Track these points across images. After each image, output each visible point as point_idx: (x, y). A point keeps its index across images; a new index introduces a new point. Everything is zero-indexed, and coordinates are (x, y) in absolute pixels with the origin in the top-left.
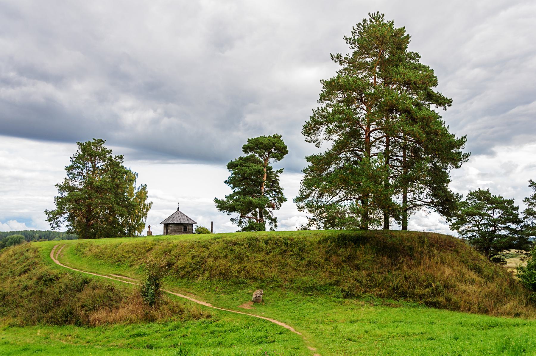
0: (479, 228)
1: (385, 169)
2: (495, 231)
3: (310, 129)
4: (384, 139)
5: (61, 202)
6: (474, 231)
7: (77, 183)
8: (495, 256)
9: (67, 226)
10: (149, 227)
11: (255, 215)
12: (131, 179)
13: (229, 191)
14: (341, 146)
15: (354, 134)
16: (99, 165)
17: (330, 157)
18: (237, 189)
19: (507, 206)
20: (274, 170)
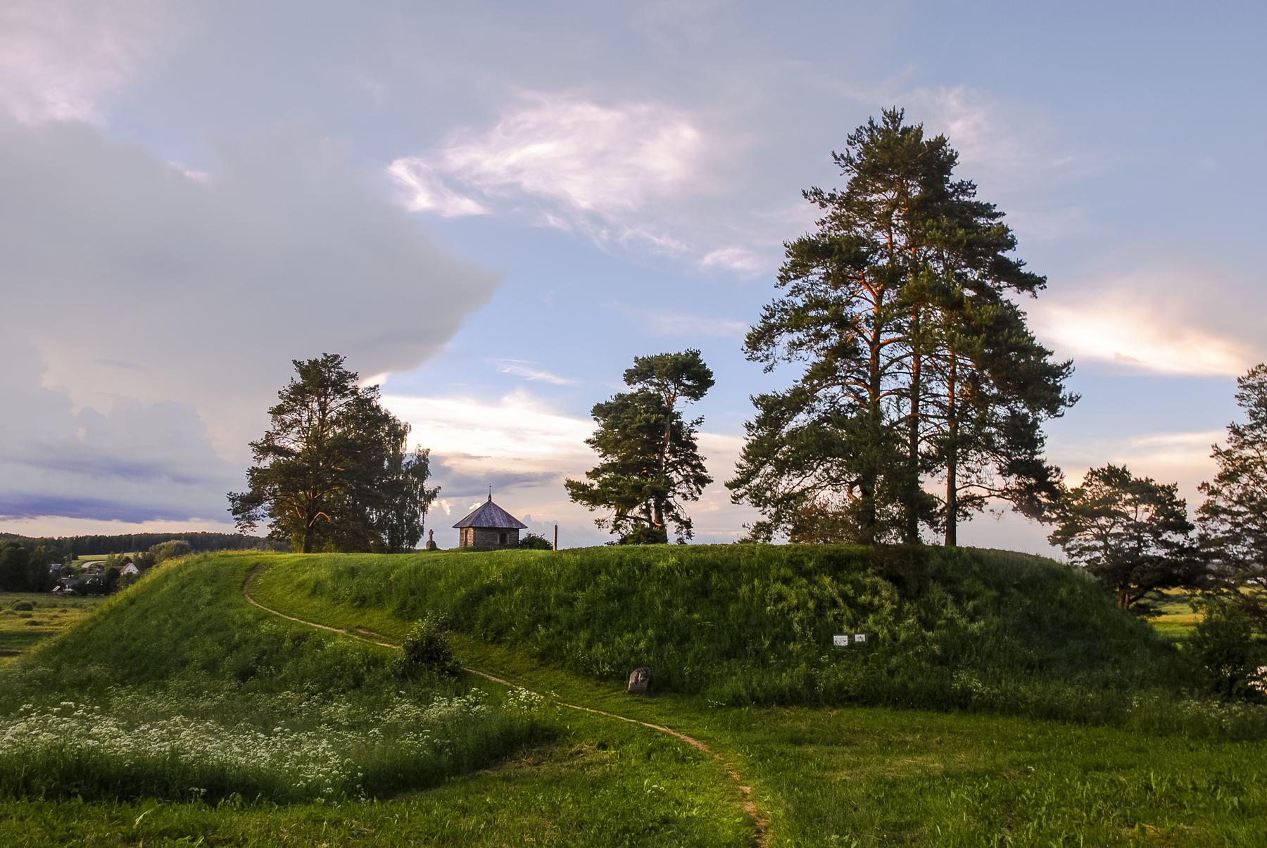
0: (1105, 541)
1: (913, 420)
2: (1139, 549)
3: (759, 339)
4: (909, 360)
5: (258, 477)
6: (1095, 549)
7: (293, 442)
8: (1142, 602)
9: (271, 526)
10: (431, 533)
11: (647, 511)
12: (398, 434)
13: (596, 459)
14: (823, 373)
15: (846, 351)
16: (333, 404)
17: (800, 399)
18: (611, 459)
19: (1160, 496)
20: (686, 419)
